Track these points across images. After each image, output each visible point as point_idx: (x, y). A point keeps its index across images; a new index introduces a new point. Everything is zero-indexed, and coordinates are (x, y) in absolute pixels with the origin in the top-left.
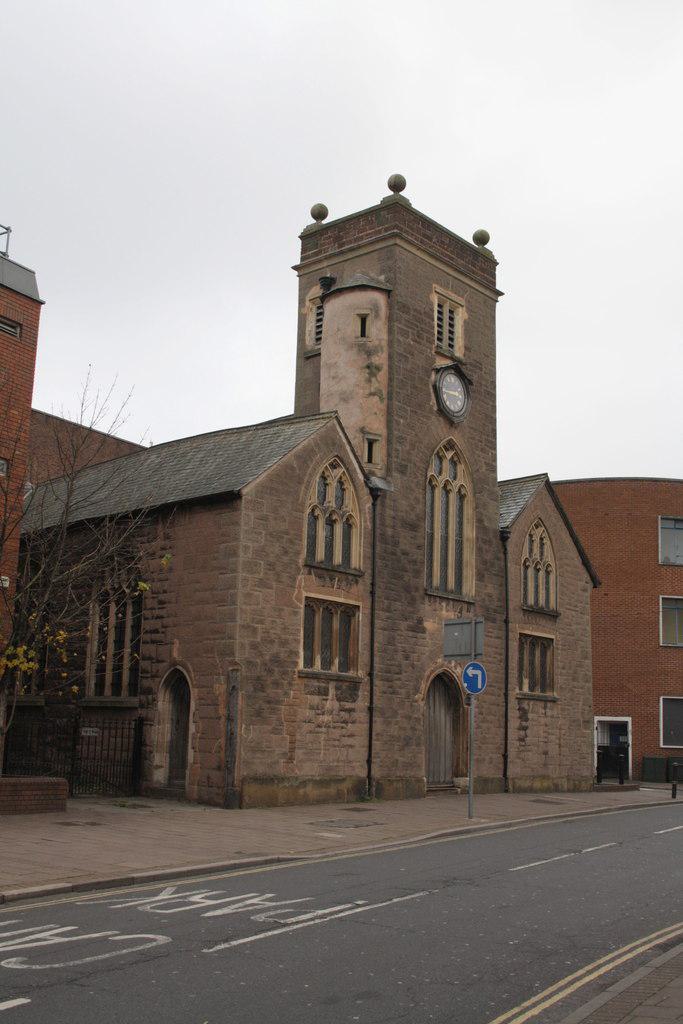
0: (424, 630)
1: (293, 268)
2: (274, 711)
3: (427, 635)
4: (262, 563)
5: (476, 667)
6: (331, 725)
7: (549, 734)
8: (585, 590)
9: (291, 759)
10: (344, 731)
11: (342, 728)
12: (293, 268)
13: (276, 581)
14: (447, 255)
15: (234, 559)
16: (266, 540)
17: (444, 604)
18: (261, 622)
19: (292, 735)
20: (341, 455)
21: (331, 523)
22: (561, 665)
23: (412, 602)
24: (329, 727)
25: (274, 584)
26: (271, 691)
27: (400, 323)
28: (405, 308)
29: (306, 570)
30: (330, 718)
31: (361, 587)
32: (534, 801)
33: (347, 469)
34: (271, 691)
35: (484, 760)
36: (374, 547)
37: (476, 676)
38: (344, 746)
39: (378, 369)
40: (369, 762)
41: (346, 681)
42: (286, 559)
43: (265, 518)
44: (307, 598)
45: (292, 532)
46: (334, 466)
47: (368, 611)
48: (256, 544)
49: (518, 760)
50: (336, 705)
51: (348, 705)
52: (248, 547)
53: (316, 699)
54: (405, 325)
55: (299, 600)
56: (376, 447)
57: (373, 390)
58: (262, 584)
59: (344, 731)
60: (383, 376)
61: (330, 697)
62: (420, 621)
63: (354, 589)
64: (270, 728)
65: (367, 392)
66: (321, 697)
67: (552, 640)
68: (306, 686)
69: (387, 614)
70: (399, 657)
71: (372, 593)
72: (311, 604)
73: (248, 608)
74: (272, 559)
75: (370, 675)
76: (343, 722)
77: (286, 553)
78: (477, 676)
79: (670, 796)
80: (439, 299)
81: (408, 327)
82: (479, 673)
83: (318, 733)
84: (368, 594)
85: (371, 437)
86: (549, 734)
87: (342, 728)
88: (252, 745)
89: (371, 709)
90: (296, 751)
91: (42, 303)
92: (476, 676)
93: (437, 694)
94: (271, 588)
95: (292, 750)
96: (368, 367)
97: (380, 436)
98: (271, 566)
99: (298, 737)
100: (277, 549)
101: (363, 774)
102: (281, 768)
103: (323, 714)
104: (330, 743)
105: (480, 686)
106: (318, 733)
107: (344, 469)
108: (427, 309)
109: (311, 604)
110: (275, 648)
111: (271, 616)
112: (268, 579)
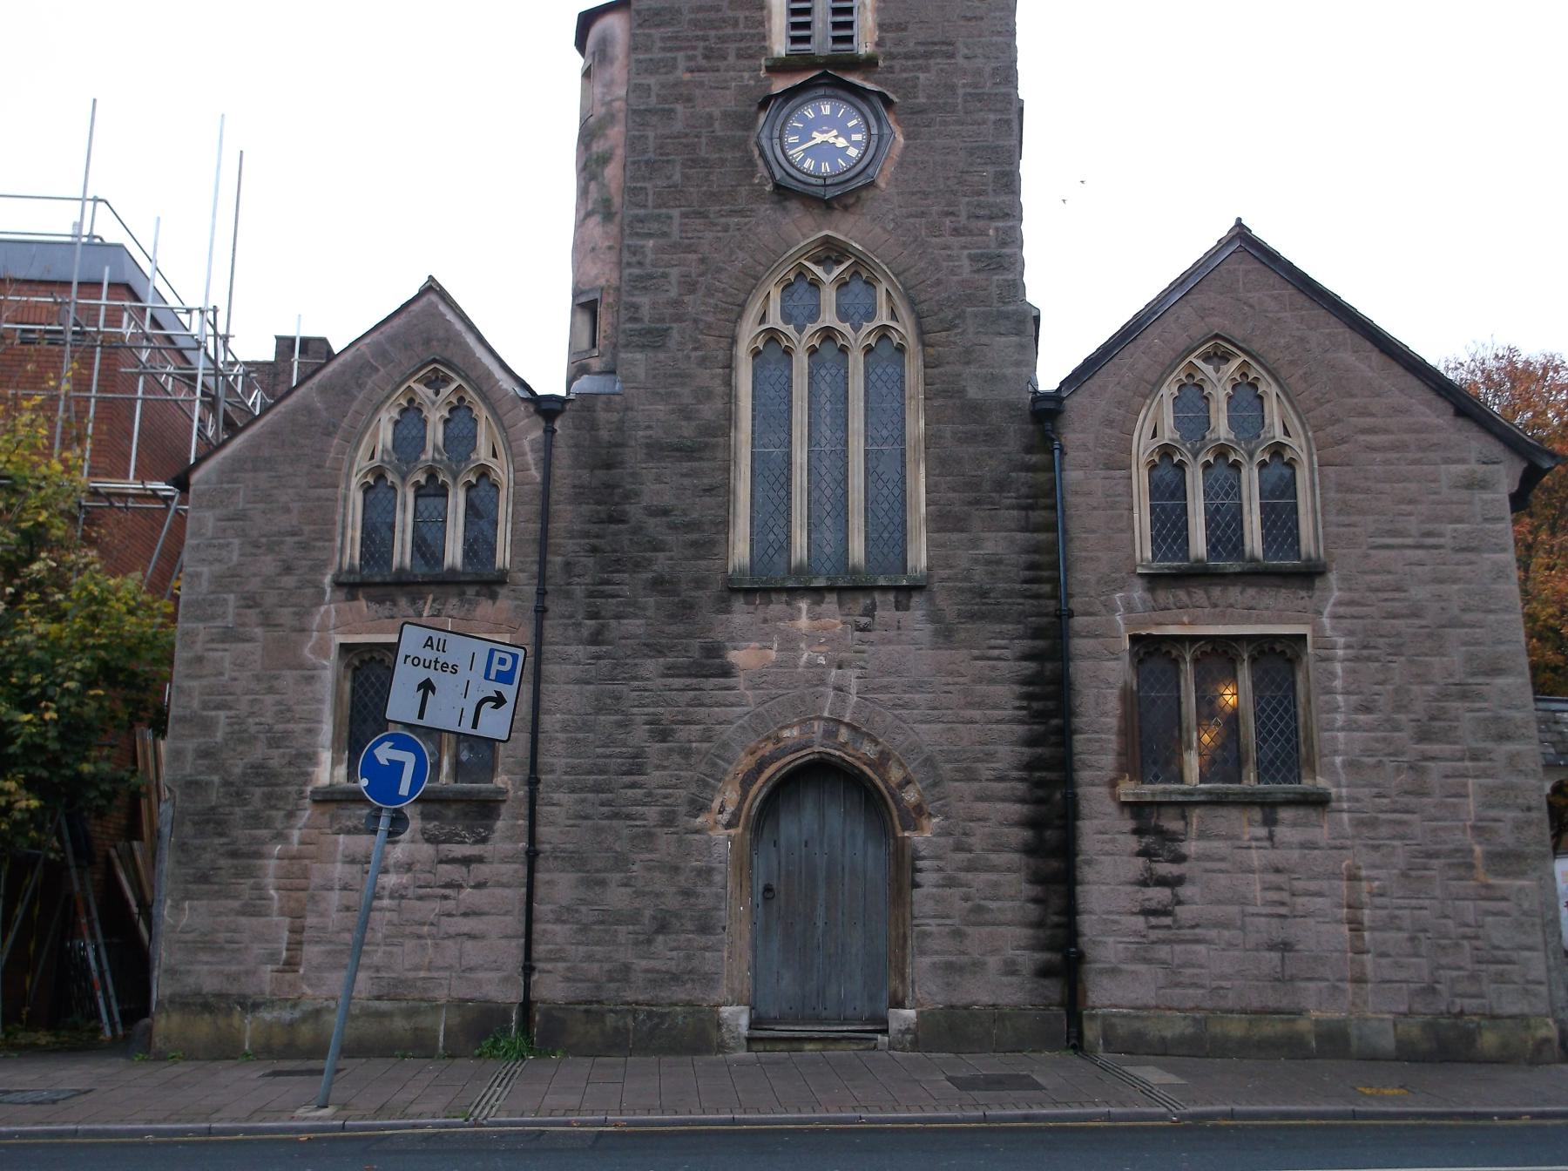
0: (727, 671)
1: (1239, 219)
2: (249, 873)
3: (740, 681)
6: (410, 893)
8: (1475, 484)
9: (291, 965)
10: (450, 905)
11: (445, 897)
13: (262, 625)
15: (725, 617)
17: (804, 605)
21: (432, 490)
23: (686, 610)
26: (241, 835)
30: (405, 878)
33: (466, 378)
34: (241, 835)
37: (398, 766)
40: (528, 969)
41: (456, 801)
42: (289, 581)
43: (241, 516)
45: (307, 529)
48: (217, 567)
49: (1142, 968)
52: (198, 575)
54: (663, 49)
55: (321, 650)
59: (450, 905)
64: (236, 904)
67: (1302, 638)
68: (334, 818)
69: (593, 649)
73: (194, 683)
74: (254, 585)
75: (533, 782)
81: (671, 50)
82: (409, 759)
88: (188, 937)
89: (532, 856)
90: (306, 948)
92: (398, 766)
95: (295, 945)
98: (250, 601)
100: (268, 564)
102: (266, 978)
110: (258, 752)
111: (252, 692)
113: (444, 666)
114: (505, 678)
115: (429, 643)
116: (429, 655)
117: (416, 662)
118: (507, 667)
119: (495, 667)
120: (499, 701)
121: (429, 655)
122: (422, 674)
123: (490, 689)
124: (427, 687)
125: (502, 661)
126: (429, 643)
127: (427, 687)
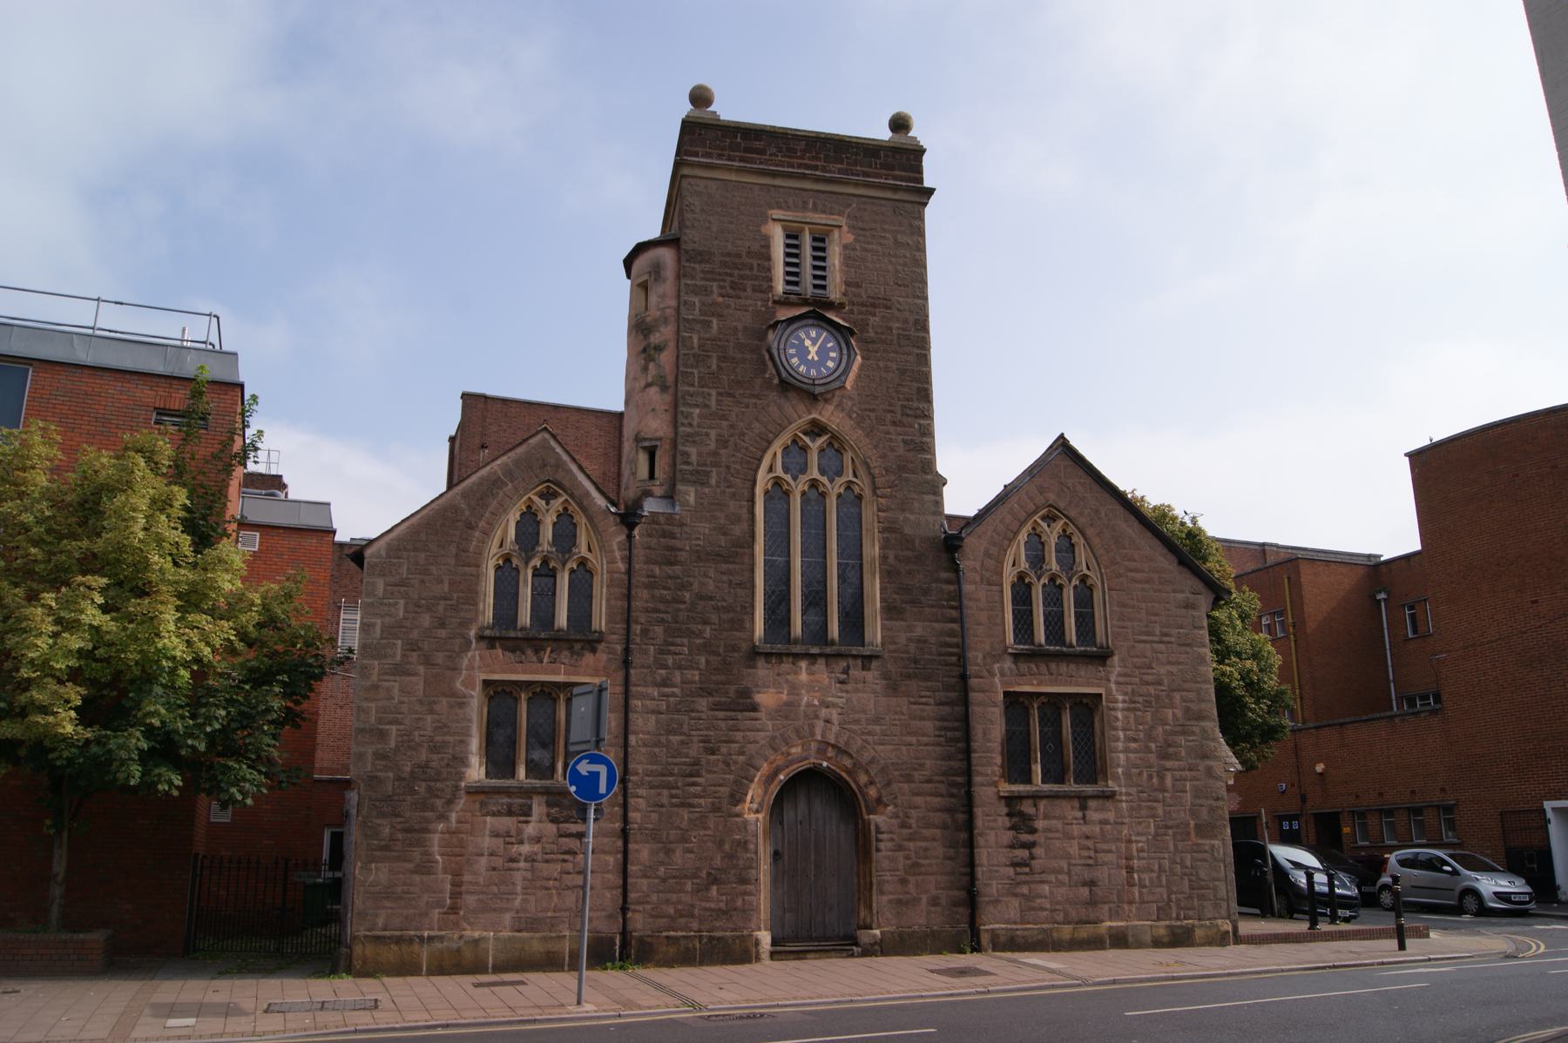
0: (754, 708)
1: (934, 190)
3: (761, 715)
4: (400, 642)
5: (595, 759)
6: (539, 857)
10: (569, 866)
12: (934, 190)
16: (406, 611)
18: (397, 722)
20: (560, 476)
24: (534, 860)
25: (421, 669)
27: (693, 278)
28: (701, 256)
30: (536, 848)
31: (603, 656)
32: (939, 972)
33: (572, 496)
35: (916, 901)
36: (629, 597)
39: (659, 349)
44: (487, 683)
46: (548, 496)
47: (619, 689)
51: (574, 828)
53: (507, 823)
54: (703, 279)
56: (658, 454)
57: (650, 380)
58: (399, 670)
60: (666, 358)
61: (534, 818)
62: (746, 693)
63: (589, 658)
64: (410, 866)
65: (643, 384)
66: (514, 819)
71: (626, 664)
72: (499, 693)
77: (442, 625)
78: (598, 774)
79: (1397, 947)
80: (785, 229)
81: (708, 280)
82: (603, 770)
83: (511, 869)
85: (647, 444)
87: (565, 861)
88: (377, 889)
91: (930, 192)
92: (596, 775)
94: (416, 674)
96: (644, 350)
97: (660, 439)
98: (412, 646)
99: (467, 878)
103: (521, 842)
104: (538, 883)
105: (603, 789)
106: (511, 869)
107: (565, 497)
108: (756, 247)
109: (499, 693)
110: (423, 755)
111: (417, 712)
112: (408, 663)
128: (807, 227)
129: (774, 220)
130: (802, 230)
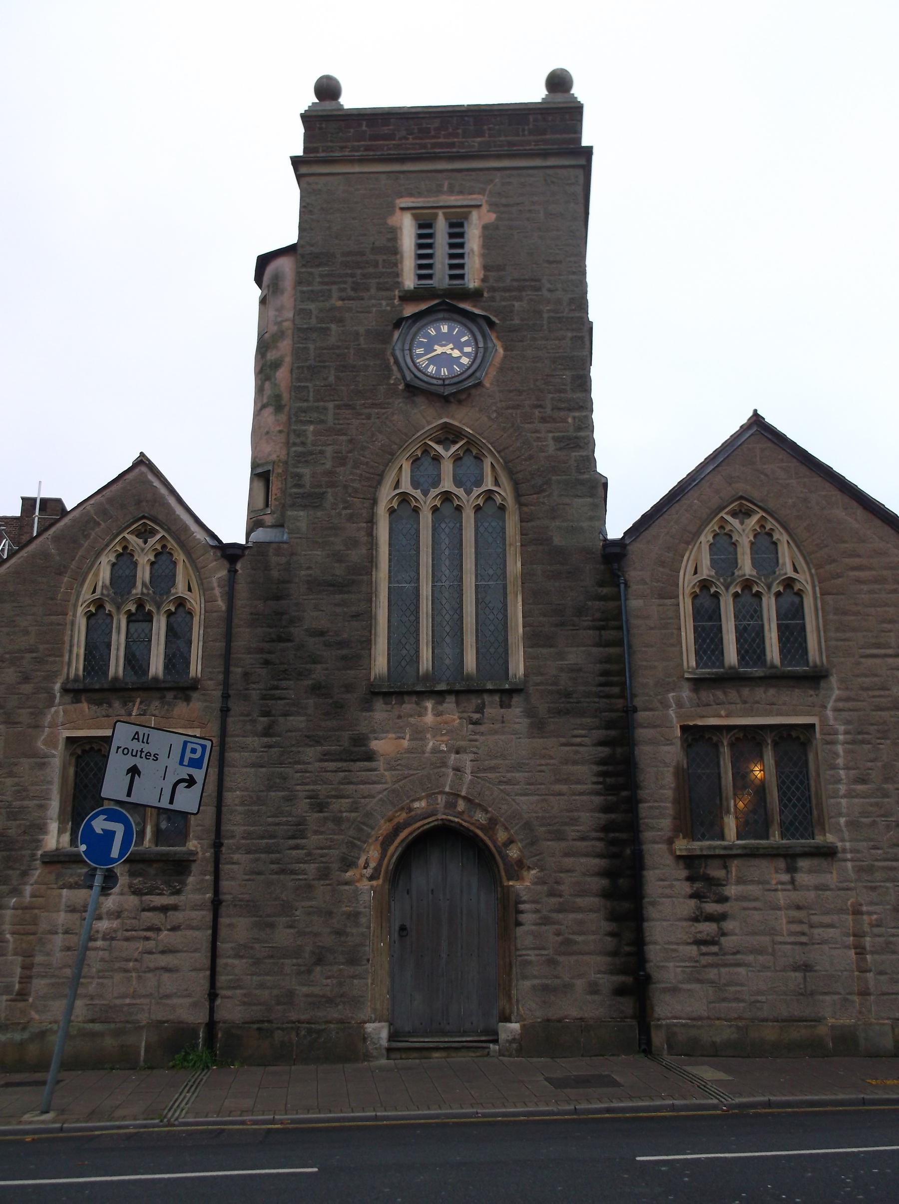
0: (370, 757)
3: (381, 764)
7: (812, 926)
10: (151, 944)
11: (147, 939)
14: (441, 145)
17: (429, 705)
19: (28, 955)
22: (324, 126)
29: (68, 698)
30: (115, 924)
33: (168, 530)
37: (110, 835)
38: (150, 970)
42: (27, 688)
45: (41, 647)
50: (132, 901)
59: (151, 944)
68: (58, 876)
69: (265, 739)
70: (302, 806)
75: (217, 845)
76: (149, 929)
80: (416, 217)
81: (327, 284)
82: (119, 829)
84: (217, 713)
86: (812, 926)
89: (216, 904)
90: (35, 981)
93: (597, 843)
95: (26, 979)
99: (39, 959)
101: (200, 1017)
113: (148, 755)
114: (196, 763)
115: (136, 737)
116: (136, 746)
117: (126, 751)
118: (197, 756)
119: (188, 755)
120: (191, 782)
121: (136, 746)
122: (130, 761)
123: (184, 773)
124: (134, 771)
125: (194, 751)
126: (136, 737)
127: (134, 771)
128: (440, 213)
129: (402, 209)
130: (435, 216)
